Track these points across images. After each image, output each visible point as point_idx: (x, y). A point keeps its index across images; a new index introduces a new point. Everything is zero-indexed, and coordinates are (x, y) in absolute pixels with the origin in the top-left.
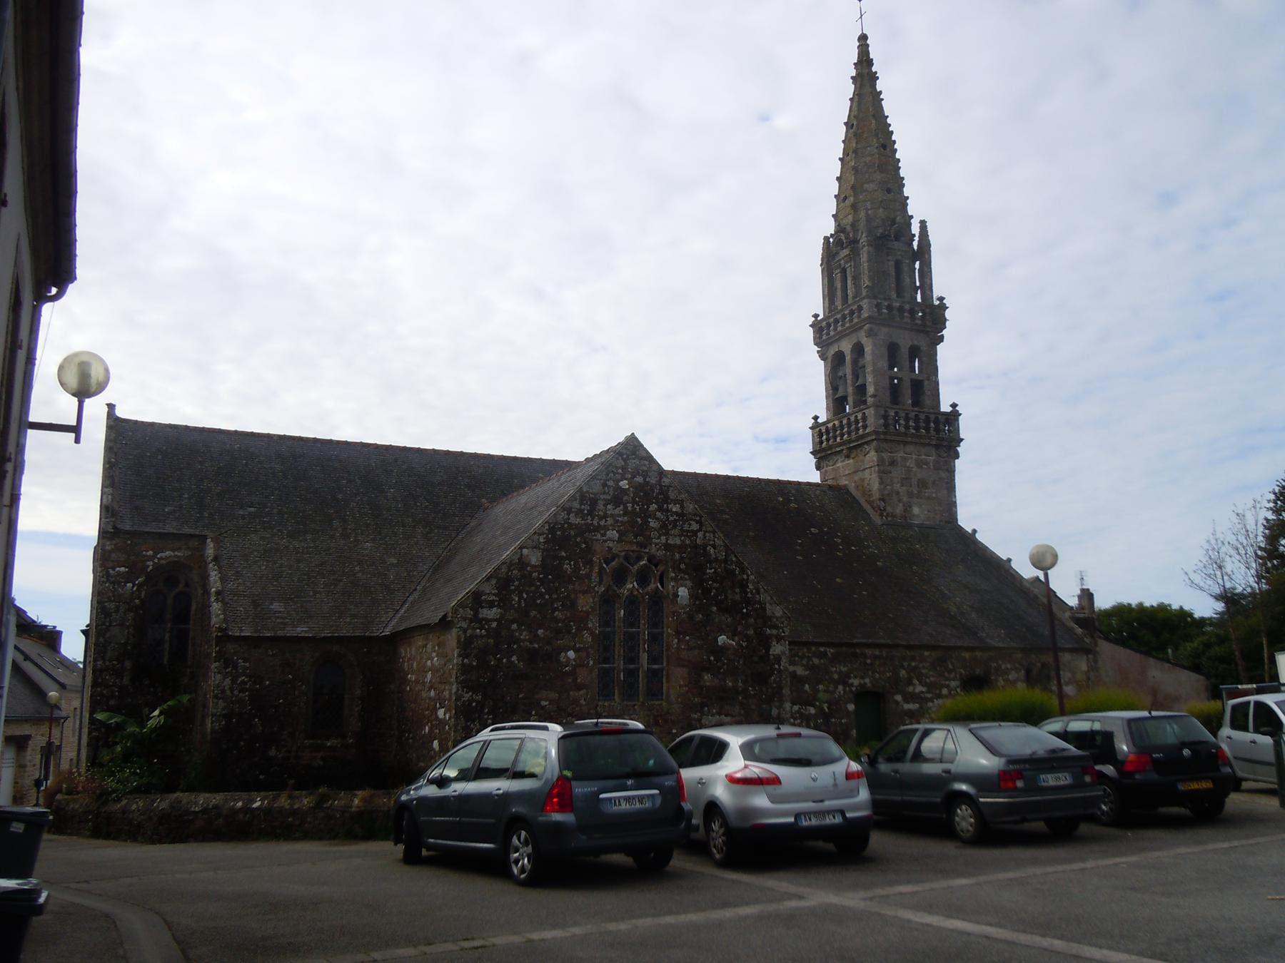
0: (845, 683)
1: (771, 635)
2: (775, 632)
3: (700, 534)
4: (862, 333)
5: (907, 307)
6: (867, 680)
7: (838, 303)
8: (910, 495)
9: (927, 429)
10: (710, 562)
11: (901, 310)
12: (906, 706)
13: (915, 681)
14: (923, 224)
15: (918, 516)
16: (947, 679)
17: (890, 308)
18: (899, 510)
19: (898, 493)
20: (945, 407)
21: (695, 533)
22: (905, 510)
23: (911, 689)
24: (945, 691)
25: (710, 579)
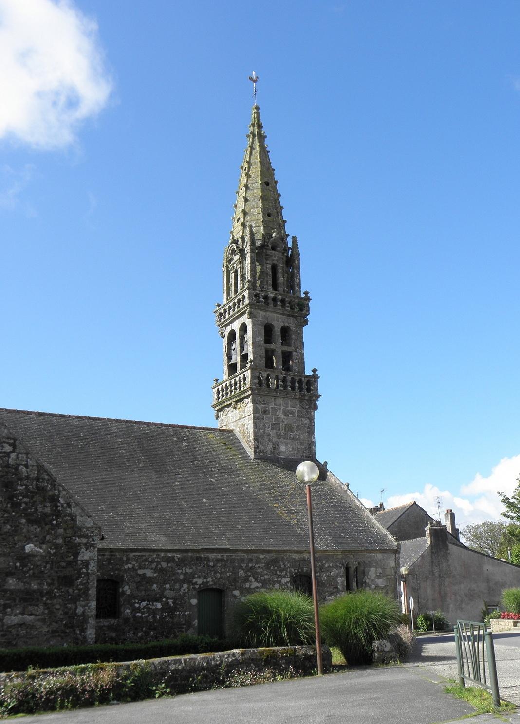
0: (189, 582)
1: (80, 543)
2: (84, 540)
3: (13, 456)
4: (246, 316)
5: (280, 297)
6: (209, 579)
7: (232, 295)
8: (279, 436)
9: (293, 388)
10: (21, 479)
11: (274, 299)
14: (295, 240)
15: (284, 452)
16: (279, 576)
17: (266, 297)
18: (270, 447)
19: (269, 435)
20: (308, 372)
21: (8, 454)
23: (247, 585)
25: (21, 494)
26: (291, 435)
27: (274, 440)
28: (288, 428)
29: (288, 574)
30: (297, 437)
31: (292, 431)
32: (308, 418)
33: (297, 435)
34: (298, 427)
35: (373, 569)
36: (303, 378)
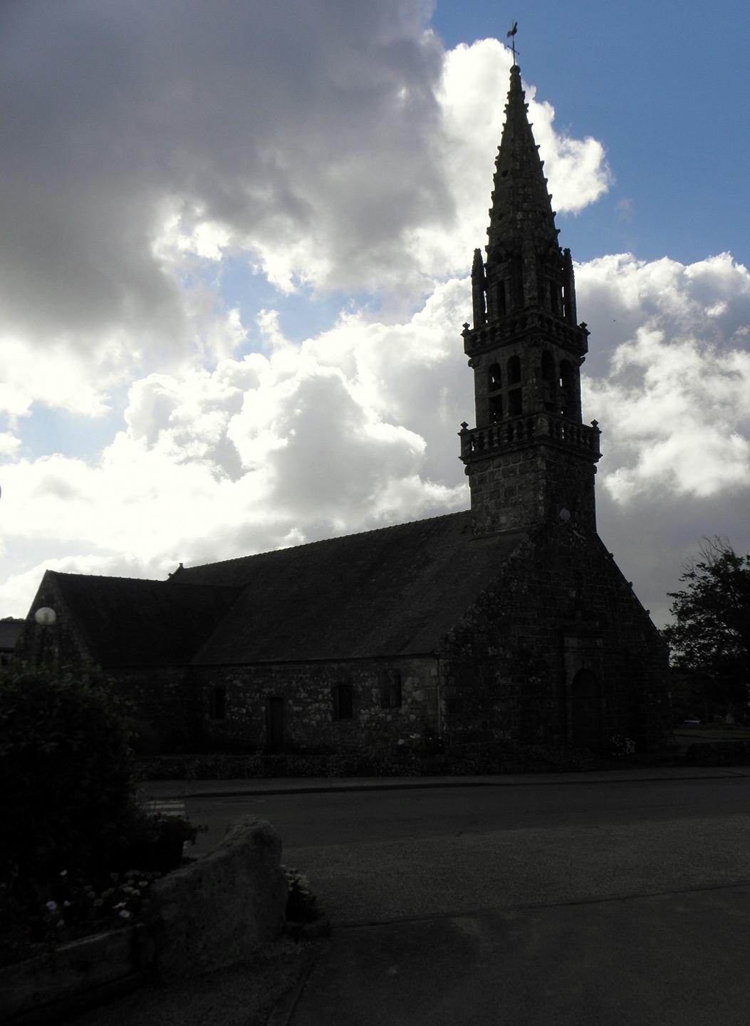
6: (273, 689)
12: (296, 709)
13: (301, 689)
19: (487, 507)
22: (494, 522)
24: (320, 697)
26: (512, 500)
27: (493, 512)
28: (510, 491)
29: (329, 684)
30: (520, 500)
31: (513, 495)
32: (533, 471)
33: (519, 498)
34: (520, 487)
35: (410, 679)
36: (522, 420)
